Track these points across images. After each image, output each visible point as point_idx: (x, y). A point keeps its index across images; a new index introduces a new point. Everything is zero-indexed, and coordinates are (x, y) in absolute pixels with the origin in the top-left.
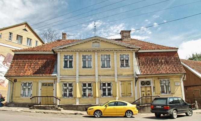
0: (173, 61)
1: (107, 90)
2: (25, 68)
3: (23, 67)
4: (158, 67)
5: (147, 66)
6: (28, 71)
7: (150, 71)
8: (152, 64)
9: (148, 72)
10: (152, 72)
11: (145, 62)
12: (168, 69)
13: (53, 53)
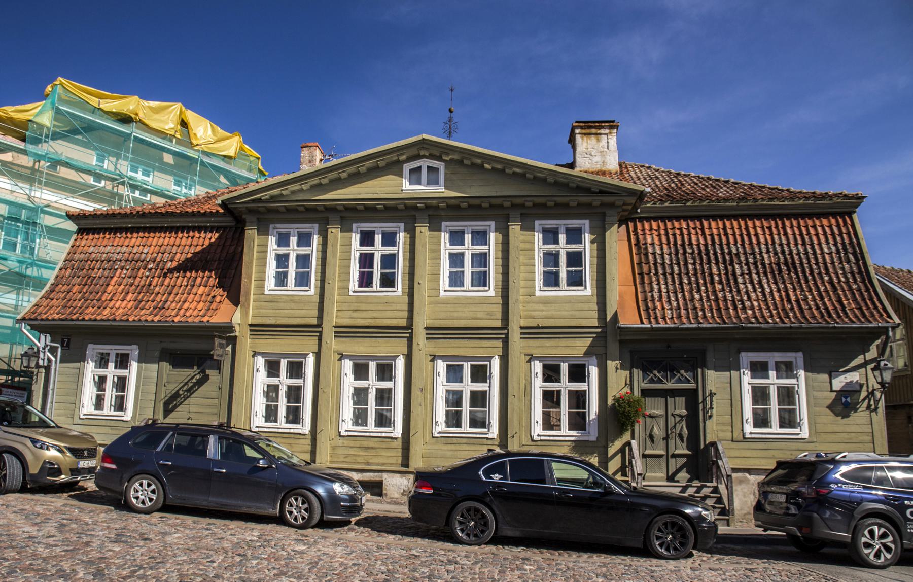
0: (825, 263)
1: (563, 259)
2: (110, 288)
3: (101, 283)
4: (739, 291)
5: (681, 283)
6: (119, 302)
7: (695, 308)
8: (711, 275)
9: (683, 312)
10: (705, 317)
11: (671, 265)
12: (793, 298)
13: (233, 224)
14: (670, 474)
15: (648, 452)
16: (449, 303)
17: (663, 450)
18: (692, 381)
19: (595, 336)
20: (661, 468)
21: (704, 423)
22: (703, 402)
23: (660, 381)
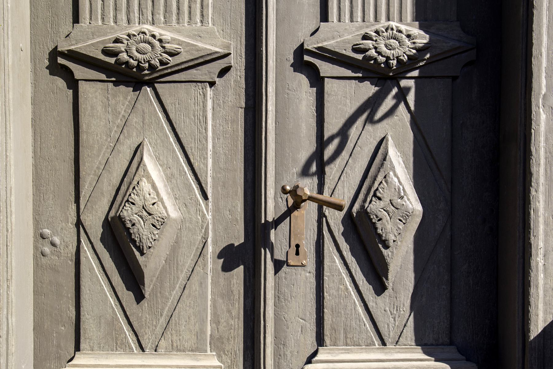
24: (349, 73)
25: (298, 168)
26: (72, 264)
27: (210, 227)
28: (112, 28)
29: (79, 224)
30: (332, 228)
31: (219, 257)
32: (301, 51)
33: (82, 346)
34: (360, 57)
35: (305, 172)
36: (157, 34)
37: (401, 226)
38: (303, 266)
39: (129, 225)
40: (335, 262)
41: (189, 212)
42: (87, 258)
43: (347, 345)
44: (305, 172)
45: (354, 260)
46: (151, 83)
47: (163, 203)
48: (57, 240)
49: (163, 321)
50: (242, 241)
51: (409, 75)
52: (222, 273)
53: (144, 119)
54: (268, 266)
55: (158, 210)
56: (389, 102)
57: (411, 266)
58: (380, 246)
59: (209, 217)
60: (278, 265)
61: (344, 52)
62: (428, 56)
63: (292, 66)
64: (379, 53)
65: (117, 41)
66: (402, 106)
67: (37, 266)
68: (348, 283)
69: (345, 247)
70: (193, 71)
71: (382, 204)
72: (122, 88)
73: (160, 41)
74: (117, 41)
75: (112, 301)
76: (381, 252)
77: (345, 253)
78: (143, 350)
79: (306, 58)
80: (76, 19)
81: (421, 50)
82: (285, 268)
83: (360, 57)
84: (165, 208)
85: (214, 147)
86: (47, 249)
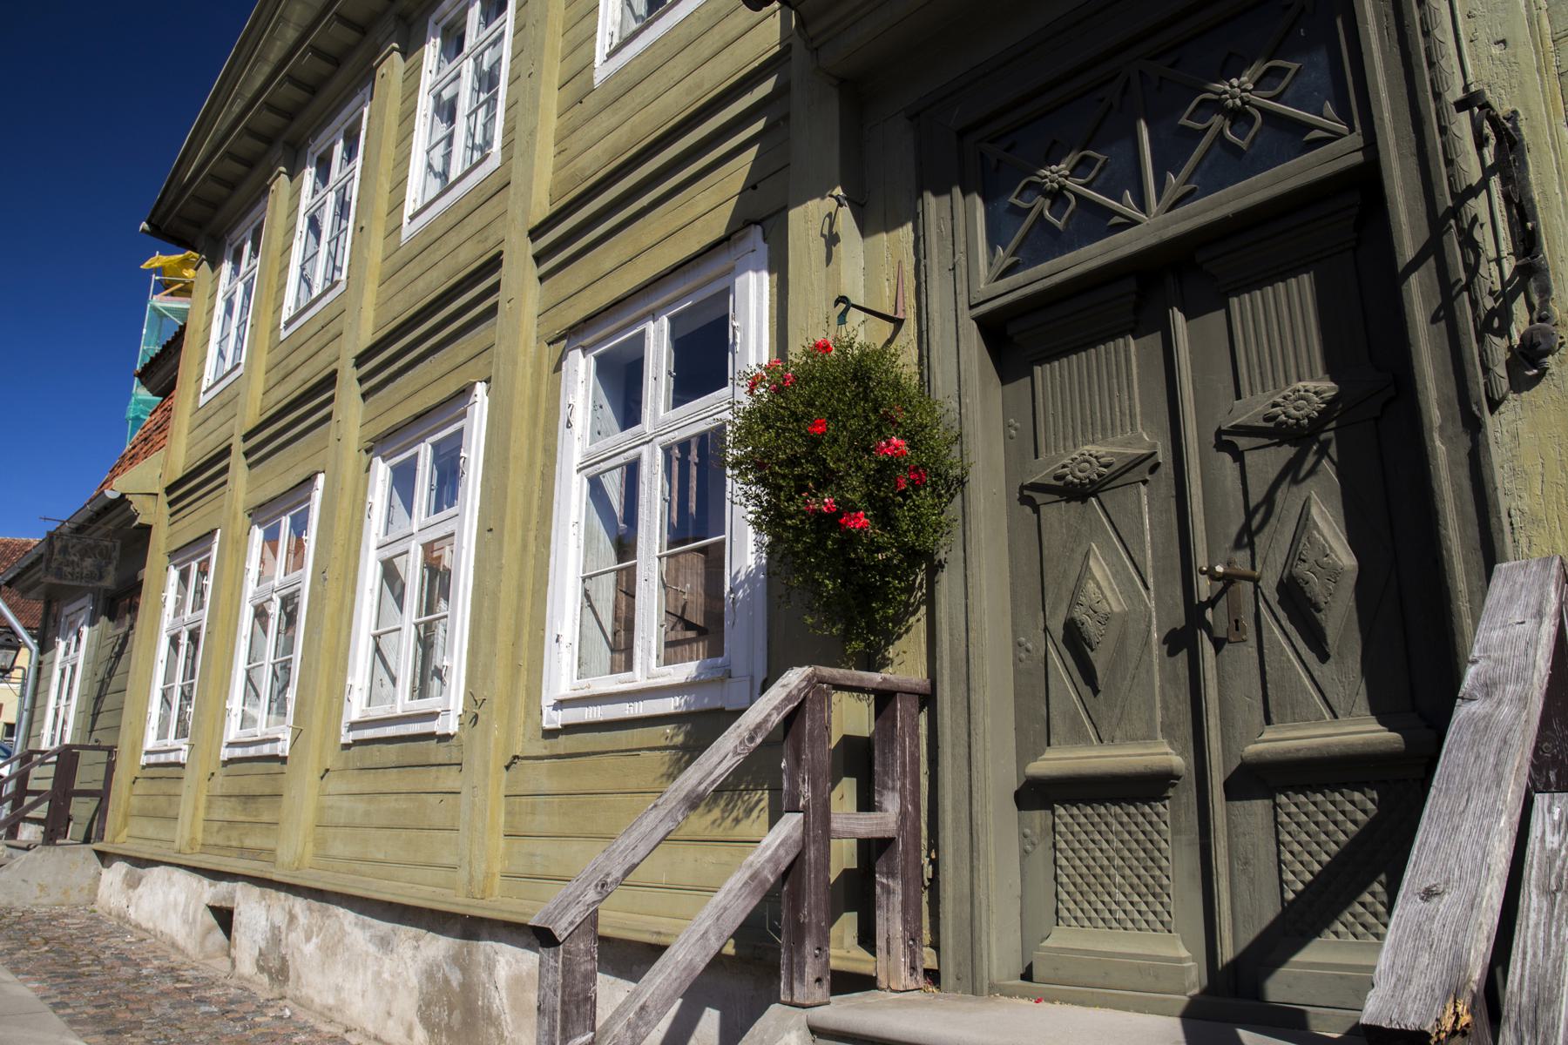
14: (1227, 953)
15: (1057, 761)
16: (412, 255)
17: (1169, 731)
18: (1328, 119)
19: (759, 126)
20: (1157, 892)
21: (1474, 426)
22: (1433, 249)
23: (1098, 222)
24: (1266, 441)
25: (1230, 543)
26: (1042, 666)
27: (1154, 614)
28: (1062, 455)
29: (1046, 629)
30: (1267, 598)
31: (1164, 643)
32: (1219, 432)
33: (1052, 741)
34: (1271, 425)
35: (1238, 545)
36: (1093, 452)
37: (1331, 586)
38: (1244, 641)
39: (1080, 625)
40: (1274, 632)
41: (1133, 604)
42: (1053, 659)
43: (1295, 721)
44: (1238, 545)
45: (1293, 628)
46: (1094, 494)
47: (1107, 600)
48: (1030, 646)
49: (1117, 710)
50: (1183, 624)
51: (1327, 428)
52: (1167, 659)
53: (1091, 526)
54: (1205, 646)
55: (1103, 608)
56: (1310, 460)
57: (1355, 626)
58: (1313, 610)
59: (1152, 605)
60: (1218, 644)
61: (1256, 424)
62: (1340, 406)
63: (1215, 447)
64: (1289, 417)
65: (1064, 466)
66: (1325, 462)
67: (1017, 672)
68: (1290, 654)
69: (1282, 614)
70: (1127, 475)
71: (1307, 566)
72: (1073, 504)
73: (1096, 457)
74: (1064, 466)
75: (1074, 696)
76: (1314, 616)
77: (1283, 622)
78: (1101, 741)
79: (1225, 438)
80: (1037, 457)
81: (1331, 403)
82: (1227, 646)
83: (1271, 425)
84: (1109, 604)
85: (1151, 538)
86: (1023, 655)
